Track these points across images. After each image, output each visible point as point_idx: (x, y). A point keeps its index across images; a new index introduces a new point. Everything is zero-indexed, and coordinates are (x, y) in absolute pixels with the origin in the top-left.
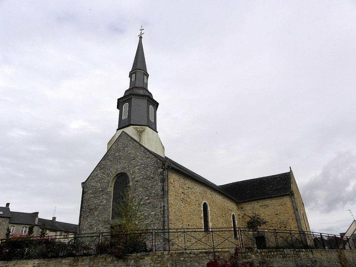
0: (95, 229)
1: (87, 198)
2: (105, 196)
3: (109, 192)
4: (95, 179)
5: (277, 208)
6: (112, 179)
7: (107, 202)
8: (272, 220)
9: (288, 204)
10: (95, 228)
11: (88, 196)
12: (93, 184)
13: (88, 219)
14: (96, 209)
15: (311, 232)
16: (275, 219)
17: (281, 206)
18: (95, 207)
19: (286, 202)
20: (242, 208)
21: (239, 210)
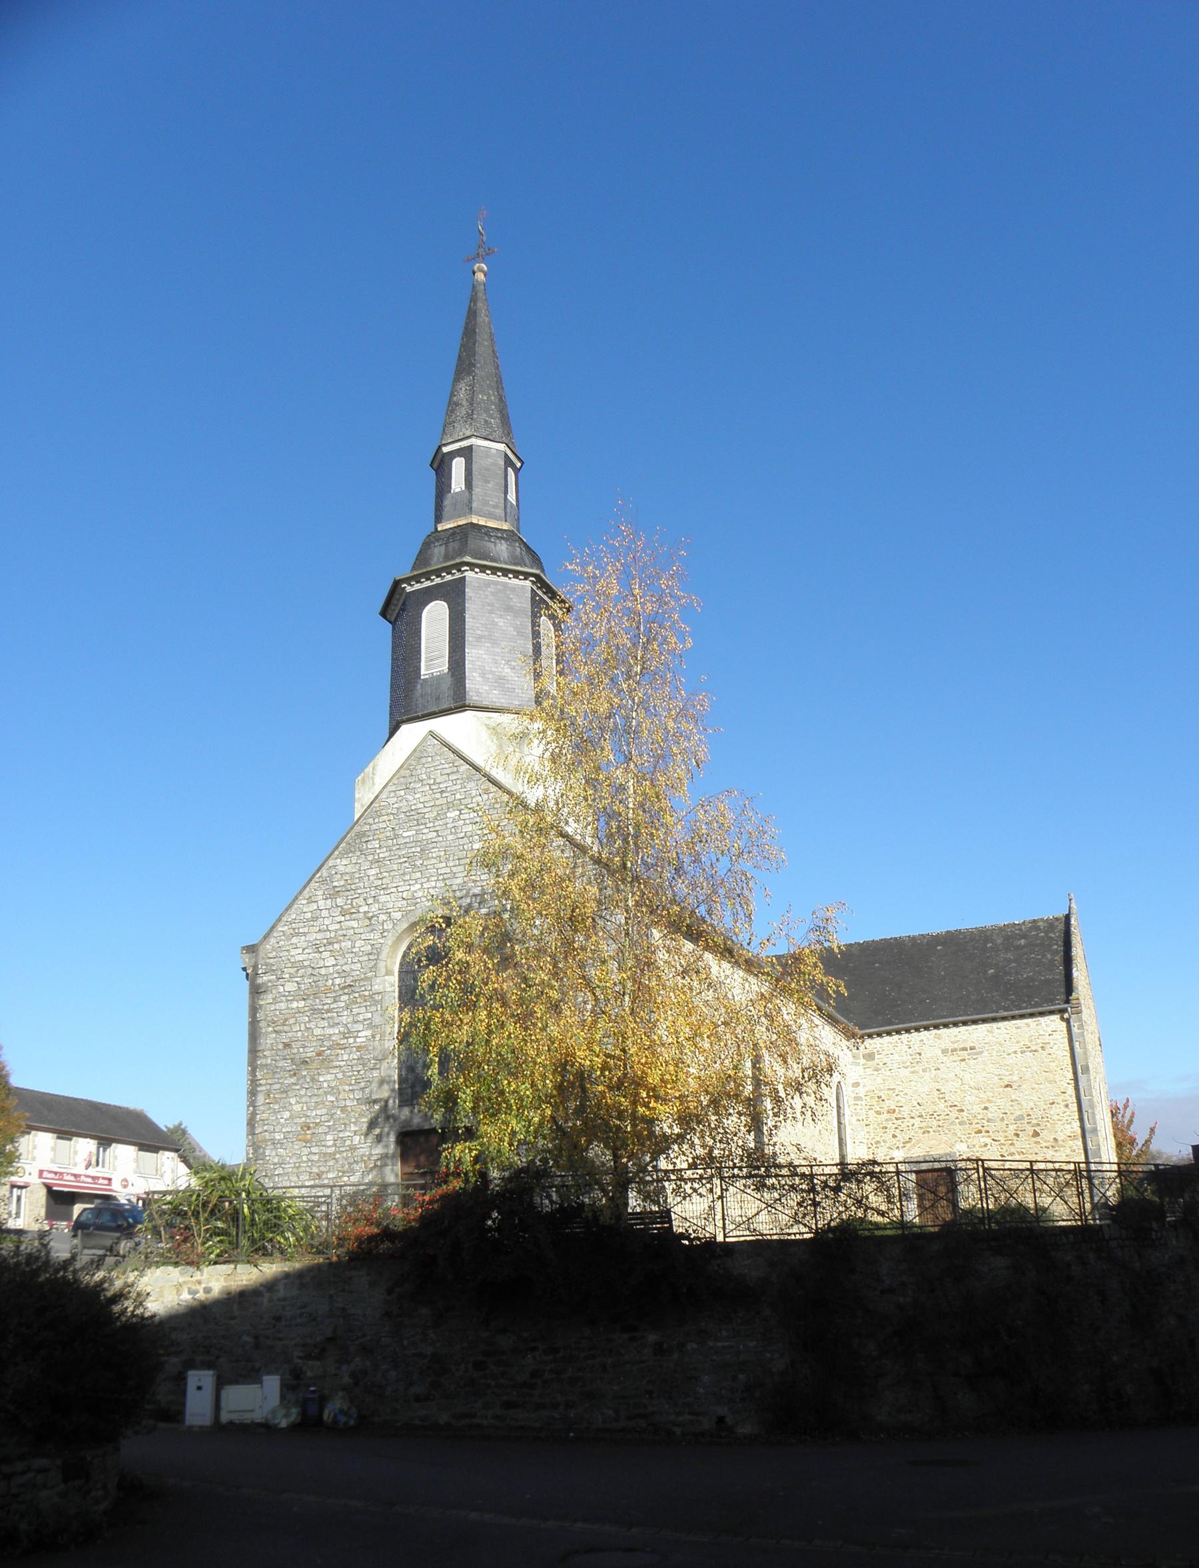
0: (330, 1143)
1: (276, 1015)
2: (363, 1010)
3: (379, 993)
4: (305, 934)
5: (1010, 1060)
6: (390, 943)
7: (373, 1036)
8: (986, 1108)
9: (1056, 1047)
10: (329, 1137)
11: (283, 1006)
12: (297, 955)
13: (293, 1101)
14: (325, 1062)
15: (597, 861)
16: (999, 1102)
17: (1028, 1054)
18: (319, 1054)
19: (1047, 1039)
20: (870, 1057)
21: (858, 1064)
